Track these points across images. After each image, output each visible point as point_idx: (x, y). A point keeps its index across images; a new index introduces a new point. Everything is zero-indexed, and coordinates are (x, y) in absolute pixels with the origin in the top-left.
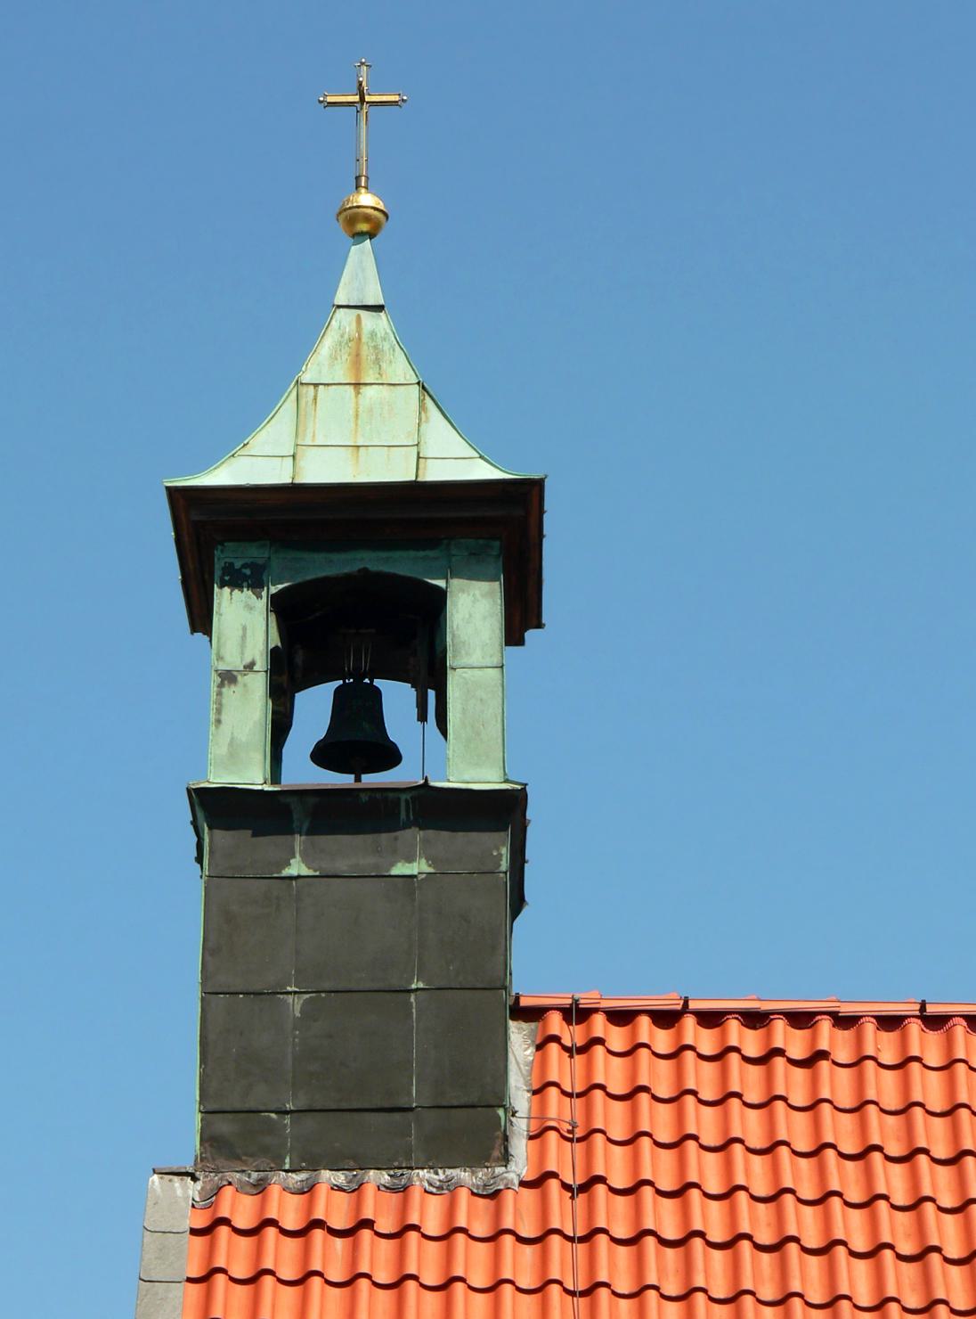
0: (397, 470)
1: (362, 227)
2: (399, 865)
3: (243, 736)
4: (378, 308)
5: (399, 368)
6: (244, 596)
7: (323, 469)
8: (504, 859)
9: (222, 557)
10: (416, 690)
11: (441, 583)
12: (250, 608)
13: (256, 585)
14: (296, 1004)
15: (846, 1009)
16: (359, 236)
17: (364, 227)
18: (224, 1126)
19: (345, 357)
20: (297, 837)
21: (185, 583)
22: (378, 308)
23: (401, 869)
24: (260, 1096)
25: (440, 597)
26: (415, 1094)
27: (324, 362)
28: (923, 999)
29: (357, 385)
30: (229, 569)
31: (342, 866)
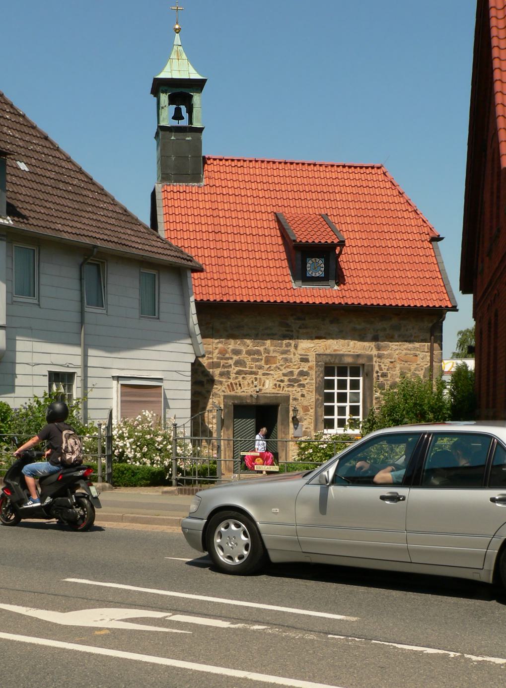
0: (186, 77)
1: (177, 31)
2: (184, 106)
3: (165, 117)
4: (180, 45)
5: (184, 56)
6: (164, 95)
7: (176, 75)
8: (485, 659)
9: (161, 88)
10: (186, 107)
11: (192, 94)
12: (165, 97)
13: (166, 93)
14: (173, 158)
15: (245, 159)
16: (178, 33)
17: (177, 31)
18: (164, 176)
19: (176, 53)
20: (173, 133)
21: (152, 88)
22: (180, 45)
23: (187, 139)
24: (169, 172)
25: (192, 96)
26: (190, 172)
27: (173, 56)
28: (459, 311)
29: (178, 59)
30: (162, 90)
31: (179, 138)
